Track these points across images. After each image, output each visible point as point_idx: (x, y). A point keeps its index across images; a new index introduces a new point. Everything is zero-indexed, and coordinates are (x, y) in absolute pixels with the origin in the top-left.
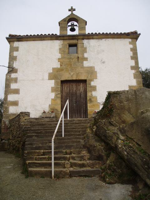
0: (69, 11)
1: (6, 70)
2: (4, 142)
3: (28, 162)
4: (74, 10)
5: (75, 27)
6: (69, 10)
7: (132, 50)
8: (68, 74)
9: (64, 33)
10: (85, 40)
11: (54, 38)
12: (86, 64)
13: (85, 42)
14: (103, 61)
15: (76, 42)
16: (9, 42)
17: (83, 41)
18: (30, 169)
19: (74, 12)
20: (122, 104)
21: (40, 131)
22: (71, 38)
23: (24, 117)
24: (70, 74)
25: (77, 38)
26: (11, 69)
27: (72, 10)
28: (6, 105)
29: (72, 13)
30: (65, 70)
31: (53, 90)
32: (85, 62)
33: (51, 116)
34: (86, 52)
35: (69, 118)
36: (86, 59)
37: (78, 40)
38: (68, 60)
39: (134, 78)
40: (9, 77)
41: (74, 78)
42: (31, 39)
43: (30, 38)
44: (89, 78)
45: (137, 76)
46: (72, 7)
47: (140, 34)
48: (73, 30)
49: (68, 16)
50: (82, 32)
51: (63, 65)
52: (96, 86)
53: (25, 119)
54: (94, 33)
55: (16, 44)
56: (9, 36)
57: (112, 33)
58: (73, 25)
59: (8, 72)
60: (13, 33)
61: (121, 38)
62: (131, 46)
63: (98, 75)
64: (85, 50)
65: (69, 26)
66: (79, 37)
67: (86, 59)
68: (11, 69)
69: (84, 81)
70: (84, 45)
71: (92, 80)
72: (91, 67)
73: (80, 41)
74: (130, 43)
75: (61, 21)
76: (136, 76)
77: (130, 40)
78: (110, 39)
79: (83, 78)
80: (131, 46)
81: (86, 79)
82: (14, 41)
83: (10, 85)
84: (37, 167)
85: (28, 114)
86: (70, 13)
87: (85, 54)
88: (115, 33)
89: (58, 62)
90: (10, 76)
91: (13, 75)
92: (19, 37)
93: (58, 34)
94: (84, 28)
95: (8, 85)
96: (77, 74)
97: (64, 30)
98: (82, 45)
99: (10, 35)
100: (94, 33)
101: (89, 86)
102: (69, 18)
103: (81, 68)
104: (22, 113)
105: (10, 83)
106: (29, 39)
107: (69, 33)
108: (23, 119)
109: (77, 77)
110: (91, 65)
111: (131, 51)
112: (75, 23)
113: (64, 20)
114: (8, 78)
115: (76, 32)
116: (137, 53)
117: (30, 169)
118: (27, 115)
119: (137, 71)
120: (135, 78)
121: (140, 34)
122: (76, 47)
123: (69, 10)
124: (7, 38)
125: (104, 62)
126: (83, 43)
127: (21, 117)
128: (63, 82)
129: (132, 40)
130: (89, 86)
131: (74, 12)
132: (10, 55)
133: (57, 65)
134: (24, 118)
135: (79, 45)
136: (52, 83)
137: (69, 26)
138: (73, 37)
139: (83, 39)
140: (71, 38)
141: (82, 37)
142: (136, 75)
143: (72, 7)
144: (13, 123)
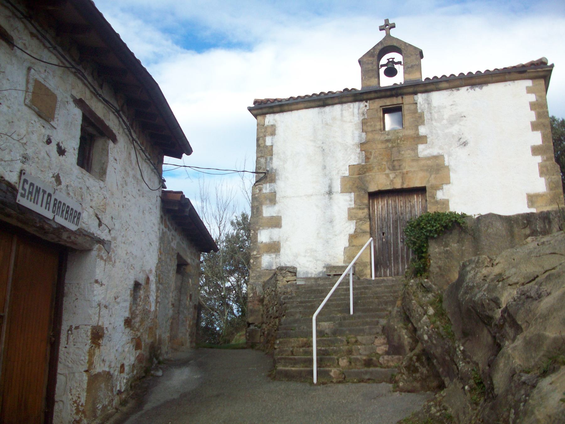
0: (381, 30)
1: (251, 179)
2: (253, 330)
3: (280, 368)
4: (393, 26)
5: (396, 67)
7: (533, 106)
8: (384, 176)
9: (373, 83)
10: (419, 95)
12: (423, 151)
13: (420, 98)
14: (462, 141)
15: (401, 102)
16: (256, 116)
17: (415, 96)
20: (448, 248)
21: (309, 304)
22: (388, 93)
23: (284, 277)
24: (387, 175)
25: (399, 91)
26: (262, 175)
28: (255, 253)
29: (388, 35)
30: (376, 168)
32: (421, 147)
33: (486, 257)
34: (423, 123)
35: (376, 276)
36: (423, 139)
37: (402, 95)
38: (384, 146)
39: (541, 176)
40: (258, 191)
41: (398, 186)
42: (299, 106)
43: (297, 103)
44: (433, 181)
45: (547, 170)
46: (387, 21)
47: (552, 66)
48: (391, 72)
49: (378, 44)
50: (413, 77)
51: (372, 157)
52: (448, 201)
53: (288, 282)
54: (466, 74)
55: (270, 119)
56: (254, 104)
57: (492, 69)
58: (393, 62)
59: (256, 182)
60: (262, 97)
61: (505, 81)
62: (532, 98)
63: (452, 175)
64: (419, 119)
65: (382, 66)
66: (405, 91)
67: (423, 139)
68: (262, 175)
69: (421, 191)
70: (418, 105)
71: (438, 187)
72: (436, 157)
73: (407, 99)
74: (529, 90)
75: (363, 56)
76: (545, 169)
78: (302, 110)
79: (417, 184)
80: (532, 98)
81: (423, 185)
82: (264, 114)
83: (262, 209)
85: (293, 271)
86: (383, 34)
87: (420, 127)
88: (439, 77)
89: (361, 150)
90: (260, 190)
91: (267, 188)
92: (273, 104)
93: (359, 87)
94: (418, 67)
95: (258, 208)
96: (404, 176)
97: (371, 77)
98: (413, 107)
99: (256, 102)
100: (466, 74)
101: (433, 201)
102: (380, 47)
103: (413, 160)
104: (281, 269)
105: (261, 204)
106: (293, 107)
107: (386, 82)
108: (282, 282)
109: (403, 183)
110: (435, 152)
111: (531, 109)
112: (397, 57)
113: (370, 54)
114: (256, 195)
115: (399, 79)
118: (291, 272)
119: (547, 158)
120: (542, 174)
121: (552, 66)
122: (400, 113)
123: (381, 29)
124: (250, 109)
125: (465, 144)
126: (416, 103)
127: (280, 278)
128: (374, 195)
129: (533, 83)
130: (433, 201)
131: (393, 33)
132: (258, 146)
134: (285, 279)
135: (405, 108)
137: (382, 66)
138: (395, 91)
139: (416, 93)
140: (388, 93)
141: (411, 90)
142: (546, 166)
144: (269, 288)
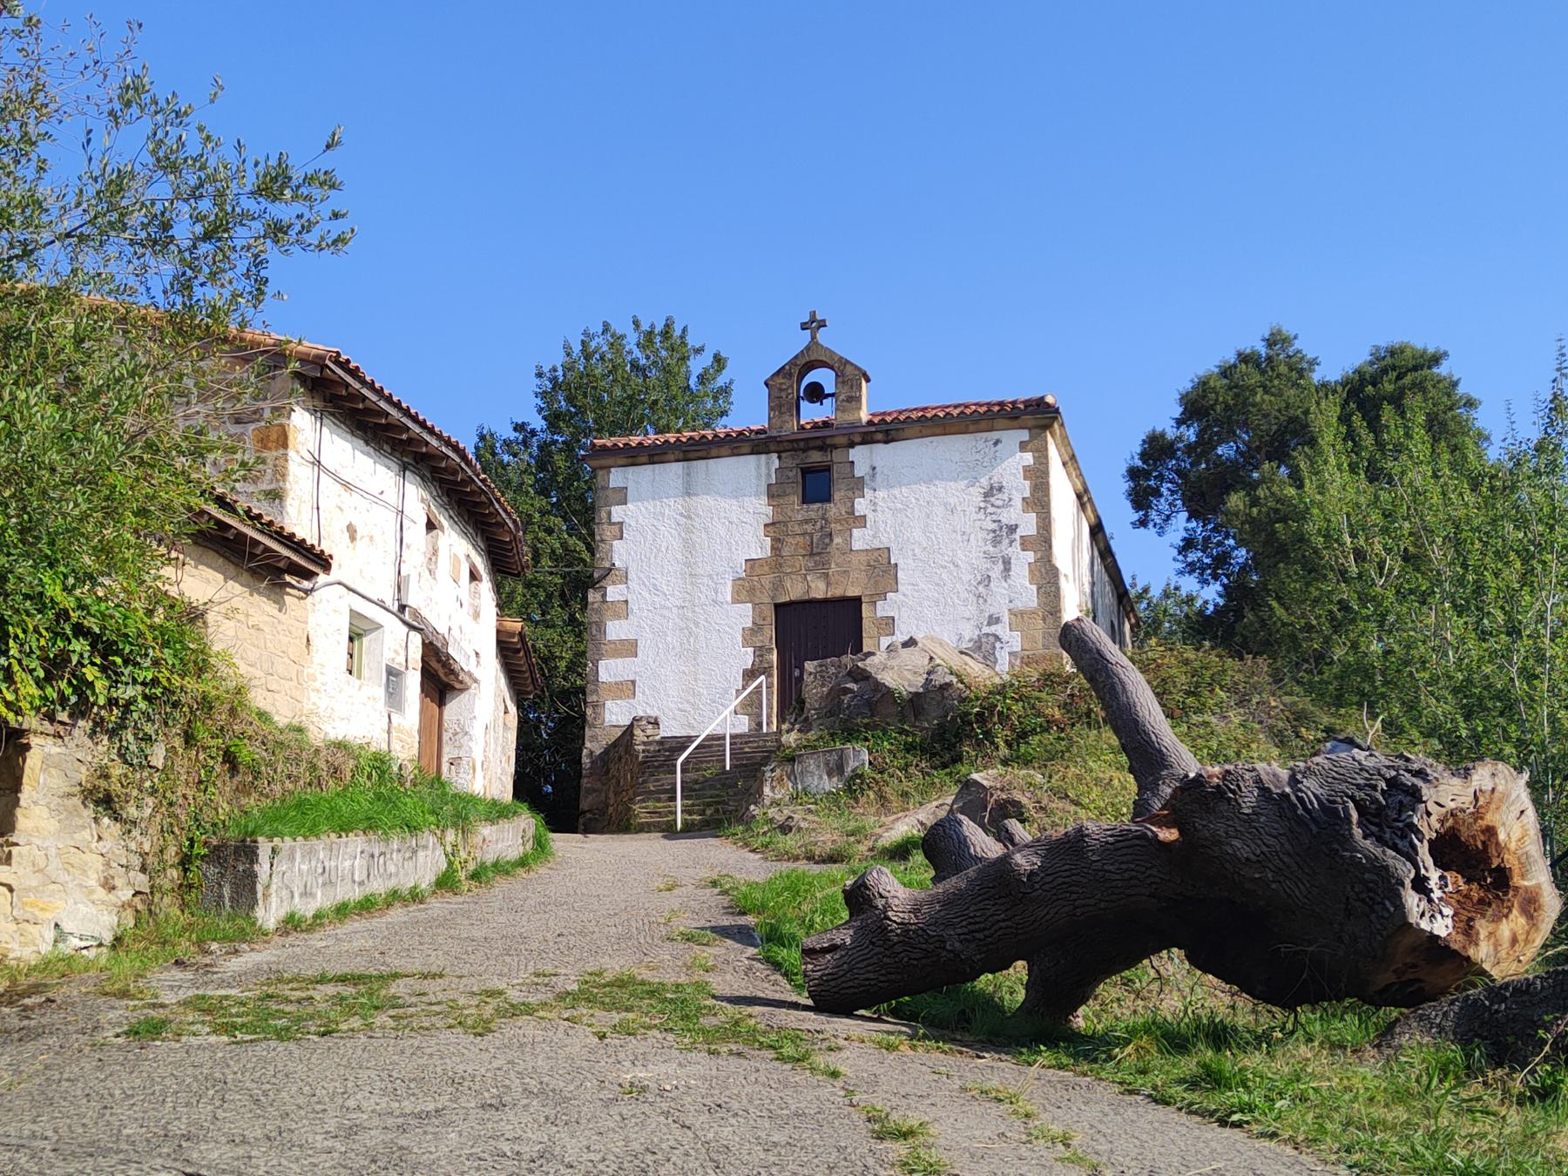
4: (822, 324)
6: (804, 327)
10: (859, 448)
11: (747, 449)
13: (858, 454)
14: (1564, 351)
18: (728, 768)
19: (822, 336)
27: (813, 324)
31: (750, 635)
36: (862, 521)
46: (813, 314)
67: (862, 521)
73: (837, 456)
77: (1024, 435)
80: (1028, 458)
84: (768, 699)
110: (884, 540)
116: (1048, 483)
117: (728, 768)
123: (804, 327)
133: (759, 547)
136: (744, 615)
143: (813, 314)
